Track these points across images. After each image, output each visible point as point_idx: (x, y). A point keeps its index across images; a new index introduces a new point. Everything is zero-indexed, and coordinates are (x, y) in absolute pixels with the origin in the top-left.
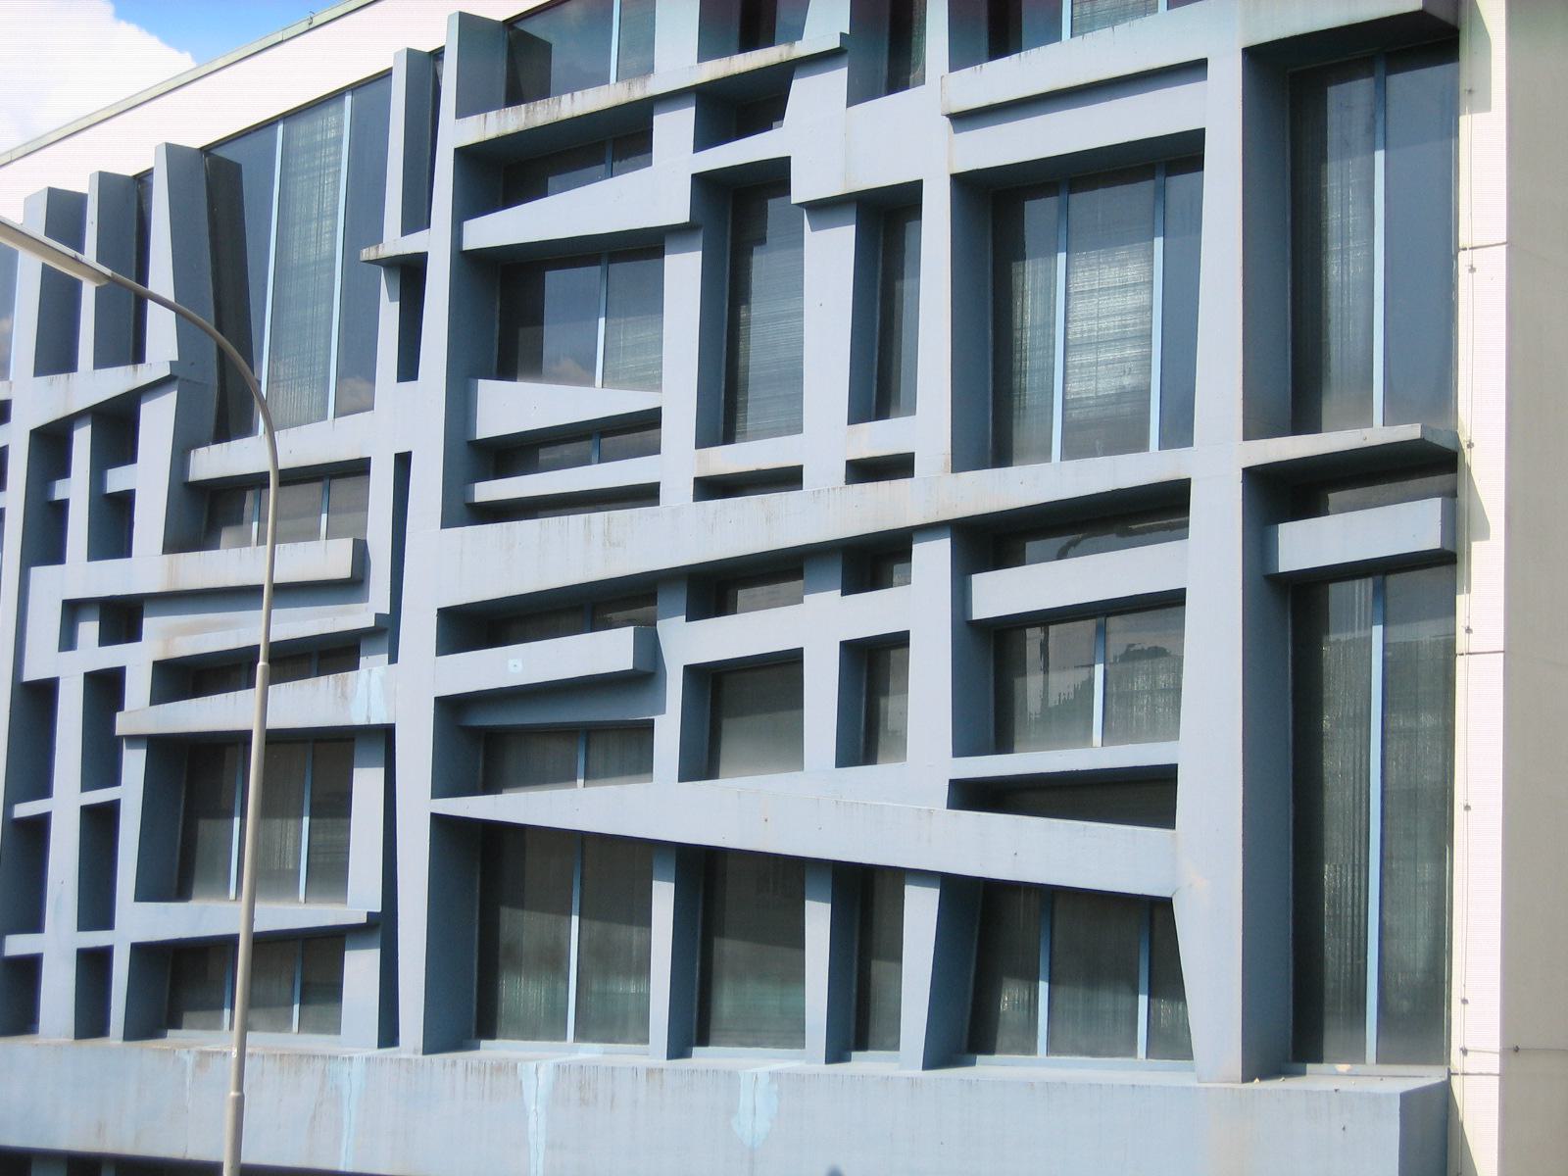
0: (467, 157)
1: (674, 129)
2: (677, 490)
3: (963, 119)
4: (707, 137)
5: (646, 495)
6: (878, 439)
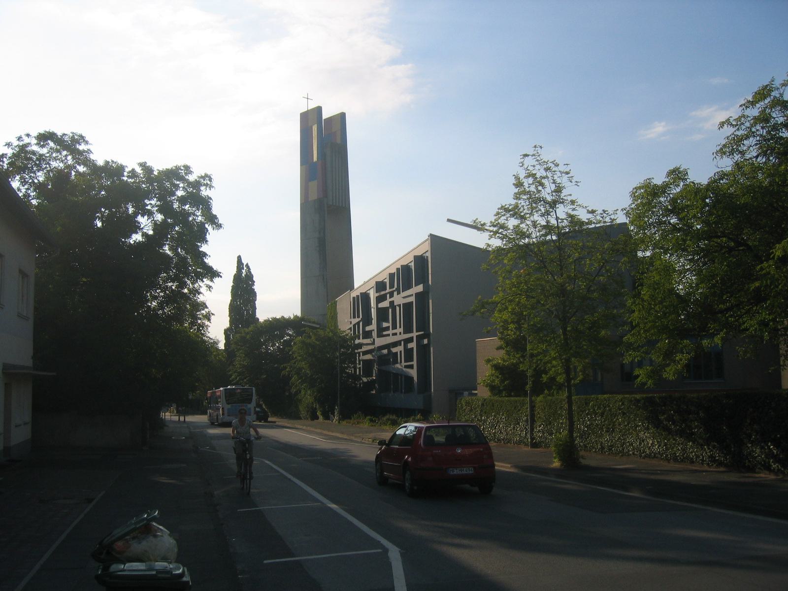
2: (391, 335)
3: (404, 298)
5: (388, 335)
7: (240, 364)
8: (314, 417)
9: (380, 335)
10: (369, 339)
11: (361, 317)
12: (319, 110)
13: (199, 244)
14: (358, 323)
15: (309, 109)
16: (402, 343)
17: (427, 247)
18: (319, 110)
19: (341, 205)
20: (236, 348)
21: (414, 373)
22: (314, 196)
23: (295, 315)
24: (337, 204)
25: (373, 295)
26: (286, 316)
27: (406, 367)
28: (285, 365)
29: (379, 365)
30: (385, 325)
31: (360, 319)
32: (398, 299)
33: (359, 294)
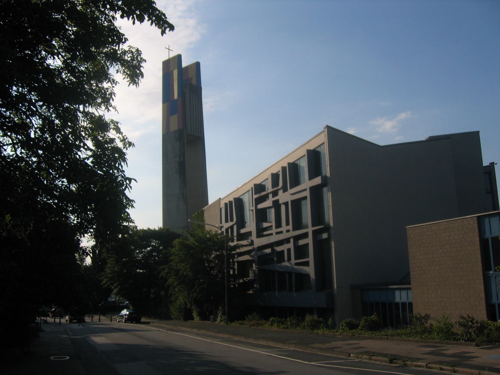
0: (256, 199)
1: (271, 196)
2: (274, 234)
3: (292, 194)
4: (273, 197)
5: (271, 234)
6: (279, 230)
7: (111, 270)
8: (188, 316)
9: (259, 235)
10: (246, 241)
11: (235, 220)
12: (179, 58)
13: (138, 10)
14: (232, 228)
15: (170, 57)
16: (292, 240)
17: (323, 138)
18: (179, 58)
19: (197, 135)
20: (107, 256)
21: (310, 270)
22: (174, 127)
23: (159, 227)
24: (195, 134)
25: (248, 201)
26: (152, 228)
27: (297, 264)
28: (163, 267)
29: (258, 264)
30: (265, 225)
31: (234, 222)
32: (284, 197)
33: (232, 199)
